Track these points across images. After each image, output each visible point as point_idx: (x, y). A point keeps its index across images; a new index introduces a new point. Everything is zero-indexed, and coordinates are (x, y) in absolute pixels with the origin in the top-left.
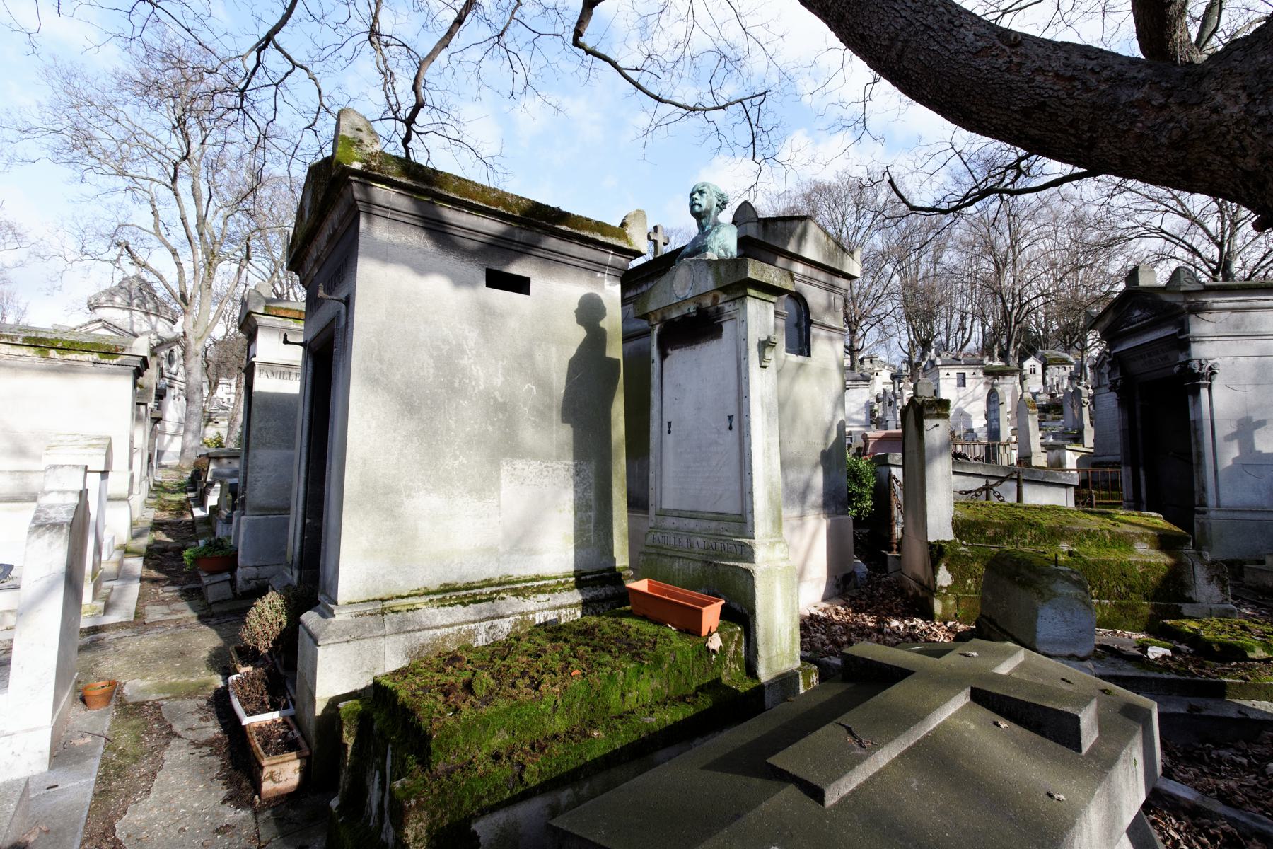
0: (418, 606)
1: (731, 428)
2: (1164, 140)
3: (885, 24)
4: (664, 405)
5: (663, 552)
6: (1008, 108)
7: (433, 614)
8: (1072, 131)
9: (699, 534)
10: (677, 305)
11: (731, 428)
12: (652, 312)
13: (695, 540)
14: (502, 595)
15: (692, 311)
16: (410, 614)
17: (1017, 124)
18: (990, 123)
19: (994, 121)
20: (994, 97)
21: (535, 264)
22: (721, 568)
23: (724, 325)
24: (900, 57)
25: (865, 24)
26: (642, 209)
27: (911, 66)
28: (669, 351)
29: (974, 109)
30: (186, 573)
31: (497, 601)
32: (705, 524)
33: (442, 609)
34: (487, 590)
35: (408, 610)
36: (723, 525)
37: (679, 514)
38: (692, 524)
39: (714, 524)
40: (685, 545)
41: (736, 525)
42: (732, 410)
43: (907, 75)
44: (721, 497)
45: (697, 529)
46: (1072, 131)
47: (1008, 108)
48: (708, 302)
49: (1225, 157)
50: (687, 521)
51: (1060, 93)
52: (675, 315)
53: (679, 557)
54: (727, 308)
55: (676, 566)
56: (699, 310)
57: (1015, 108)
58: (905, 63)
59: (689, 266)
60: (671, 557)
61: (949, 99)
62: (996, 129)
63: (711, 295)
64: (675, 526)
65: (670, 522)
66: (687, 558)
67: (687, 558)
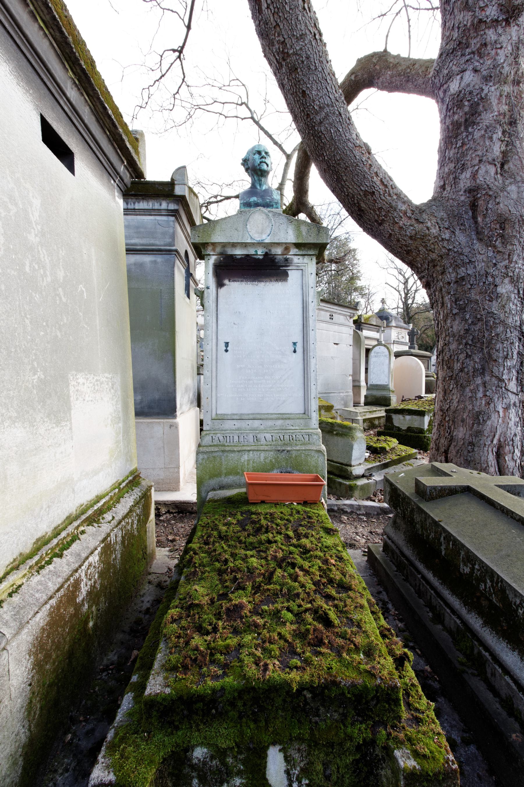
0: (19, 583)
1: (295, 351)
2: (408, 233)
3: (320, 95)
4: (219, 327)
5: (227, 449)
6: (359, 187)
7: (40, 583)
8: (378, 213)
9: (265, 430)
10: (245, 245)
11: (295, 351)
12: (214, 244)
13: (261, 436)
14: (82, 528)
15: (259, 253)
16: (16, 598)
17: (359, 197)
18: (347, 190)
19: (350, 190)
20: (356, 177)
21: (76, 139)
22: (294, 454)
23: (290, 272)
24: (321, 123)
25: (308, 86)
26: (270, 154)
27: (325, 133)
28: (226, 282)
29: (344, 179)
30: (518, 610)
31: (82, 537)
32: (270, 423)
33: (43, 572)
34: (70, 529)
35: (10, 595)
36: (288, 422)
37: (231, 418)
38: (256, 424)
39: (279, 423)
40: (251, 440)
41: (302, 421)
42: (298, 338)
43: (320, 137)
44: (284, 401)
45: (262, 427)
46: (378, 213)
47: (359, 187)
48: (278, 251)
49: (427, 250)
50: (248, 422)
51: (381, 191)
52: (239, 252)
53: (249, 451)
54: (296, 260)
55: (245, 457)
56: (266, 255)
57: (363, 189)
58: (323, 129)
59: (267, 215)
60: (238, 451)
61: (335, 165)
62: (348, 195)
63: (284, 246)
64: (236, 427)
65: (229, 425)
66: (257, 450)
67: (257, 450)
